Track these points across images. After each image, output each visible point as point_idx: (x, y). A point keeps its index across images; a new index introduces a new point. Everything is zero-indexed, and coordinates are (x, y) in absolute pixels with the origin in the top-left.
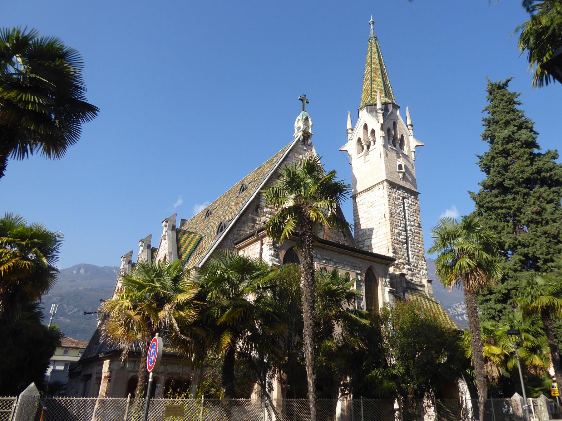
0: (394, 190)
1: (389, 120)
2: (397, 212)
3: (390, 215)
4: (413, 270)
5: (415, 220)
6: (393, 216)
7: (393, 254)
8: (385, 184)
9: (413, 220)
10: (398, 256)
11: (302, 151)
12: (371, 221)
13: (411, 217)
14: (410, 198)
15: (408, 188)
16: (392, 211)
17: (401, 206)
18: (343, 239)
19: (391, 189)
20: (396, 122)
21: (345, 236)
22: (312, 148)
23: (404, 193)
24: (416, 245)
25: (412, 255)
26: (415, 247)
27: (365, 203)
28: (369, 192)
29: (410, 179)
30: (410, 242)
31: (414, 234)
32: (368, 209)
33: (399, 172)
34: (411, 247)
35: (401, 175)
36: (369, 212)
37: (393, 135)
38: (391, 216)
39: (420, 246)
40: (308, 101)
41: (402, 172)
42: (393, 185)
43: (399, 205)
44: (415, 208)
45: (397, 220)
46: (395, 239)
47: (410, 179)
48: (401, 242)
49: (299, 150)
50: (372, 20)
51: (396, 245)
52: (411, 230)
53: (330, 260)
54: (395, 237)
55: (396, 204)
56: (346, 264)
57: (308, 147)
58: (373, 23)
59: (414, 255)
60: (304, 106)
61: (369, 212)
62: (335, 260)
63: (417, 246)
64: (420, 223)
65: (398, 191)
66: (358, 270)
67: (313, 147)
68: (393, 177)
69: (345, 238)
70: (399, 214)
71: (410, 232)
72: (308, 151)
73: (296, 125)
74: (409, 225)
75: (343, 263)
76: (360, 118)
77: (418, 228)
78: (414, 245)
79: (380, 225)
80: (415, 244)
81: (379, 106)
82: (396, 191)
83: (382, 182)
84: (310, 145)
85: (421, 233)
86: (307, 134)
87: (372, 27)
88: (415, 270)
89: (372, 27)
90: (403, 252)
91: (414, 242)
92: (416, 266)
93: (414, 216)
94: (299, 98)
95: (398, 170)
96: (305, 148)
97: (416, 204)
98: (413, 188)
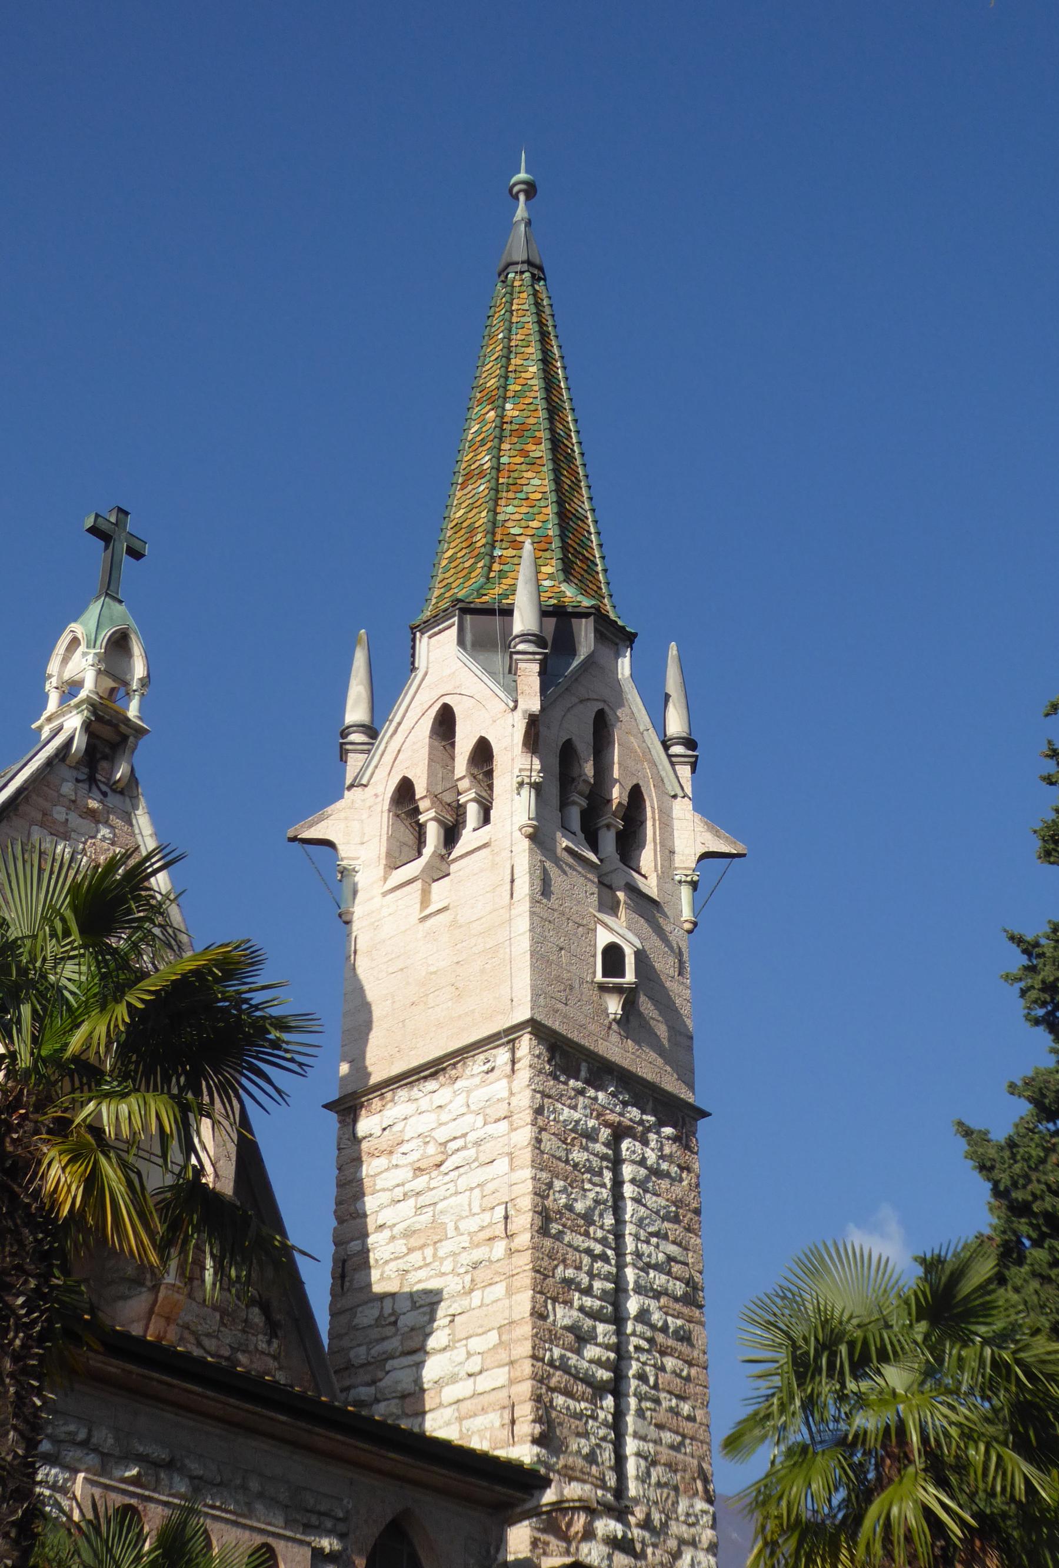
0: (572, 1082)
1: (575, 700)
2: (579, 1207)
3: (538, 1222)
4: (638, 1547)
5: (670, 1259)
6: (555, 1227)
7: (536, 1449)
8: (526, 1044)
9: (661, 1257)
10: (562, 1463)
11: (75, 820)
12: (429, 1252)
13: (654, 1240)
14: (652, 1136)
15: (650, 1077)
16: (549, 1203)
17: (600, 1174)
18: (262, 1346)
19: (556, 1078)
20: (610, 716)
21: (273, 1329)
22: (135, 807)
23: (625, 1104)
24: (665, 1404)
25: (643, 1463)
26: (662, 1416)
27: (405, 1148)
28: (431, 1085)
29: (662, 1030)
30: (634, 1383)
31: (660, 1338)
32: (421, 1182)
33: (603, 988)
34: (640, 1413)
35: (614, 1006)
36: (423, 1200)
37: (586, 782)
38: (543, 1231)
39: (686, 1408)
40: (137, 545)
41: (618, 989)
42: (564, 1054)
43: (590, 1170)
44: (678, 1191)
45: (571, 1255)
46: (551, 1363)
47: (662, 1030)
48: (588, 1380)
49: (59, 813)
50: (522, 176)
51: (560, 1400)
52: (643, 1316)
53: (170, 1465)
54: (557, 1352)
55: (576, 1166)
56: (261, 1495)
57: (113, 800)
58: (531, 190)
59: (654, 1463)
60: (112, 571)
61: (423, 1200)
62: (195, 1467)
63: (671, 1409)
64: (697, 1277)
65: (591, 1092)
66: (329, 1533)
67: (142, 803)
68: (570, 1011)
69: (275, 1343)
70: (587, 1218)
71: (640, 1328)
72: (106, 823)
73: (53, 666)
74: (639, 1290)
75: (244, 1488)
76: (420, 674)
77: (686, 1310)
78: (657, 1401)
79: (481, 1274)
80: (663, 1395)
81: (524, 620)
82: (581, 1092)
83: (508, 1036)
84: (128, 790)
85: (700, 1336)
86: (116, 726)
87: (521, 211)
88: (649, 1550)
89: (521, 211)
90: (593, 1440)
91: (656, 1387)
92: (657, 1523)
93: (665, 1237)
94: (89, 522)
95: (599, 977)
96: (93, 804)
97: (682, 1168)
98: (671, 1084)
